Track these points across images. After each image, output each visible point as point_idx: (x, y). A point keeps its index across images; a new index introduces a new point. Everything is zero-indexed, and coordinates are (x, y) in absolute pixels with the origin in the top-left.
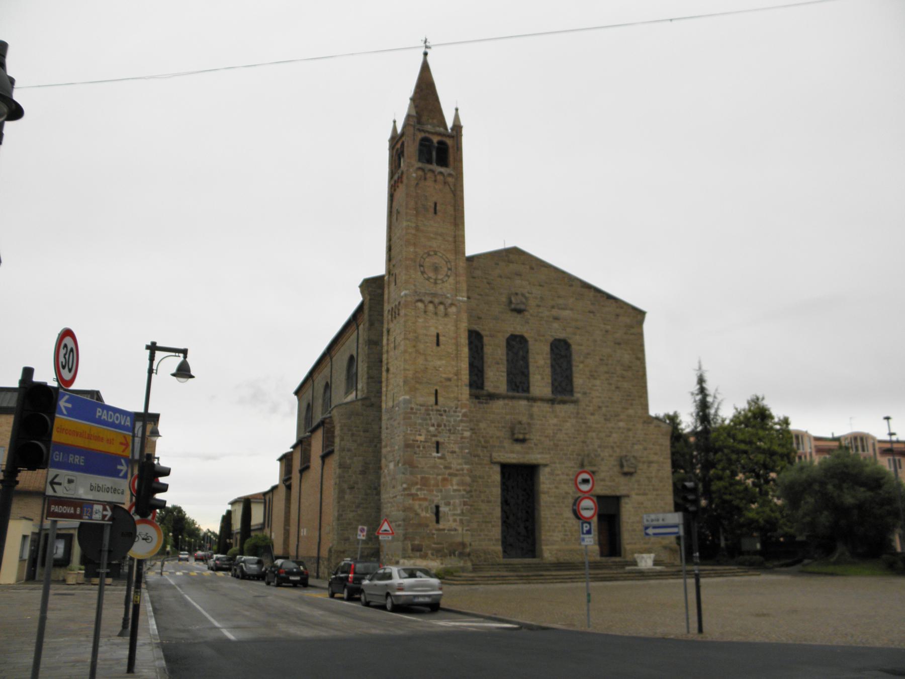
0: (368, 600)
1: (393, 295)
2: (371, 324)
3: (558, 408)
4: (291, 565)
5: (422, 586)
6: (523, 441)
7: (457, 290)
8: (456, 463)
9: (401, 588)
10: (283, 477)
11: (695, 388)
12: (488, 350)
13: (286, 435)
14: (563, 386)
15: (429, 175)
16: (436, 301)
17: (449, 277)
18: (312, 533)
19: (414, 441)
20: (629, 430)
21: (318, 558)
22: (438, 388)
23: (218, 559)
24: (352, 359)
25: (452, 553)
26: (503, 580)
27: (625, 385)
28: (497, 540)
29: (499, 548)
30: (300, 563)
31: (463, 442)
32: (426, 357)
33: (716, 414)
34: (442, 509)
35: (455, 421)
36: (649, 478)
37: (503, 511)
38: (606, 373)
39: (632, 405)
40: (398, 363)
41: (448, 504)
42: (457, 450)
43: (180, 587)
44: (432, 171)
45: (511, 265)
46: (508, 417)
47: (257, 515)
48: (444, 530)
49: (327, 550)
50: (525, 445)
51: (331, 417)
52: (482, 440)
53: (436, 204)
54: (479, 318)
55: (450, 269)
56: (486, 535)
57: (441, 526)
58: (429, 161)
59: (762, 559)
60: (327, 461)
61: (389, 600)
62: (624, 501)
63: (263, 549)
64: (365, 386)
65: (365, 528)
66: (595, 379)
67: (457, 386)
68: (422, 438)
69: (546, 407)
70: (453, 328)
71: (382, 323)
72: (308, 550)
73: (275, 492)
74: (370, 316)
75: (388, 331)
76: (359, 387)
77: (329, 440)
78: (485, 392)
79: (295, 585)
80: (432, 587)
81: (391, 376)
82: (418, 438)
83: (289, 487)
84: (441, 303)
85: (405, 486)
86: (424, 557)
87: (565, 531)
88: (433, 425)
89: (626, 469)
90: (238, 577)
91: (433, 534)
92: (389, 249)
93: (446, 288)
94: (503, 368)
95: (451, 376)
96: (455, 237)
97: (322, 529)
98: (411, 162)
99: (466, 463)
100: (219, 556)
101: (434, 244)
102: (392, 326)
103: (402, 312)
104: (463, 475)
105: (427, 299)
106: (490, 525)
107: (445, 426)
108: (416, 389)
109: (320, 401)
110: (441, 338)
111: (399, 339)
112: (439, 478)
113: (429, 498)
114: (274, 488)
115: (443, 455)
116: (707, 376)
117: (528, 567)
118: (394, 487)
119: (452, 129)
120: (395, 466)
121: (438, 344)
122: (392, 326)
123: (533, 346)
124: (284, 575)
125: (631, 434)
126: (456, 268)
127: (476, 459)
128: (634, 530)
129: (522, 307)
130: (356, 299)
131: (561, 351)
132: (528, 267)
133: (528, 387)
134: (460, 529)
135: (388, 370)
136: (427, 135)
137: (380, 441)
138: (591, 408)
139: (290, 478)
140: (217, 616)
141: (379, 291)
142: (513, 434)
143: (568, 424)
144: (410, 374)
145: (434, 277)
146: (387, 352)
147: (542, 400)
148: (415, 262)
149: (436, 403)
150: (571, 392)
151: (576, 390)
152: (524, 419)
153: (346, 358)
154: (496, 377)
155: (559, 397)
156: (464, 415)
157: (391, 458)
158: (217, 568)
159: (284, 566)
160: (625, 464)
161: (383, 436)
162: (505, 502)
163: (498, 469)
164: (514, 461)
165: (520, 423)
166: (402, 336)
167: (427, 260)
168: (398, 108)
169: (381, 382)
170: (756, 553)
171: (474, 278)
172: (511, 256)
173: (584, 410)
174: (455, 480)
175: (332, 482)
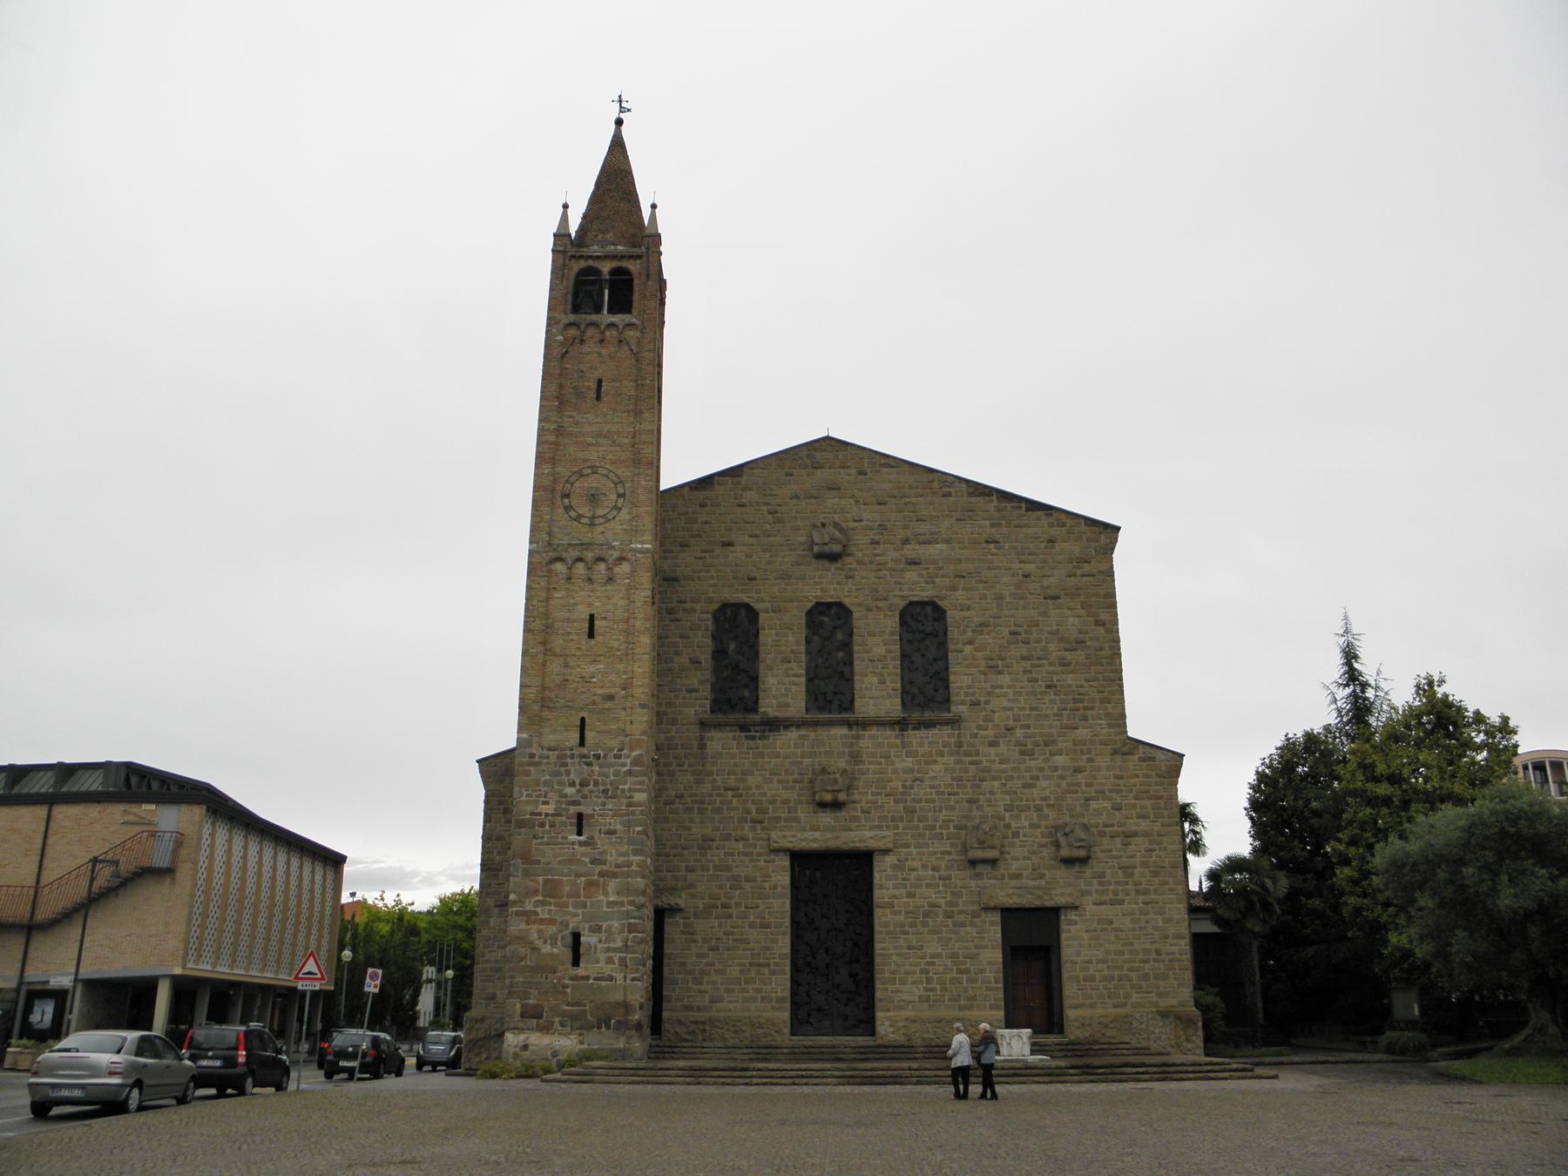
3: (914, 736)
6: (836, 805)
14: (927, 691)
16: (589, 555)
17: (620, 509)
20: (1077, 770)
22: (585, 715)
25: (603, 1022)
28: (780, 1000)
29: (786, 1015)
31: (633, 813)
35: (617, 774)
36: (1127, 870)
38: (1023, 658)
39: (1085, 718)
41: (596, 929)
42: (619, 827)
46: (807, 761)
48: (587, 978)
50: (843, 814)
53: (600, 382)
55: (620, 496)
56: (758, 990)
57: (580, 972)
59: (1418, 1036)
65: (380, 972)
66: (1000, 673)
67: (624, 709)
68: (550, 809)
69: (889, 736)
70: (622, 603)
78: (757, 718)
82: (543, 809)
86: (546, 1029)
87: (929, 981)
88: (572, 784)
89: (1065, 853)
94: (799, 668)
95: (613, 691)
99: (636, 852)
101: (593, 454)
106: (766, 970)
107: (596, 783)
108: (542, 719)
115: (591, 838)
121: (591, 635)
123: (861, 622)
124: (330, 1057)
125: (1080, 778)
127: (741, 844)
131: (924, 628)
132: (854, 471)
134: (619, 977)
136: (590, 262)
138: (990, 732)
145: (589, 514)
147: (880, 723)
148: (553, 491)
149: (582, 743)
151: (953, 698)
156: (636, 762)
162: (799, 928)
164: (815, 846)
170: (1411, 1024)
173: (975, 736)
174: (612, 885)
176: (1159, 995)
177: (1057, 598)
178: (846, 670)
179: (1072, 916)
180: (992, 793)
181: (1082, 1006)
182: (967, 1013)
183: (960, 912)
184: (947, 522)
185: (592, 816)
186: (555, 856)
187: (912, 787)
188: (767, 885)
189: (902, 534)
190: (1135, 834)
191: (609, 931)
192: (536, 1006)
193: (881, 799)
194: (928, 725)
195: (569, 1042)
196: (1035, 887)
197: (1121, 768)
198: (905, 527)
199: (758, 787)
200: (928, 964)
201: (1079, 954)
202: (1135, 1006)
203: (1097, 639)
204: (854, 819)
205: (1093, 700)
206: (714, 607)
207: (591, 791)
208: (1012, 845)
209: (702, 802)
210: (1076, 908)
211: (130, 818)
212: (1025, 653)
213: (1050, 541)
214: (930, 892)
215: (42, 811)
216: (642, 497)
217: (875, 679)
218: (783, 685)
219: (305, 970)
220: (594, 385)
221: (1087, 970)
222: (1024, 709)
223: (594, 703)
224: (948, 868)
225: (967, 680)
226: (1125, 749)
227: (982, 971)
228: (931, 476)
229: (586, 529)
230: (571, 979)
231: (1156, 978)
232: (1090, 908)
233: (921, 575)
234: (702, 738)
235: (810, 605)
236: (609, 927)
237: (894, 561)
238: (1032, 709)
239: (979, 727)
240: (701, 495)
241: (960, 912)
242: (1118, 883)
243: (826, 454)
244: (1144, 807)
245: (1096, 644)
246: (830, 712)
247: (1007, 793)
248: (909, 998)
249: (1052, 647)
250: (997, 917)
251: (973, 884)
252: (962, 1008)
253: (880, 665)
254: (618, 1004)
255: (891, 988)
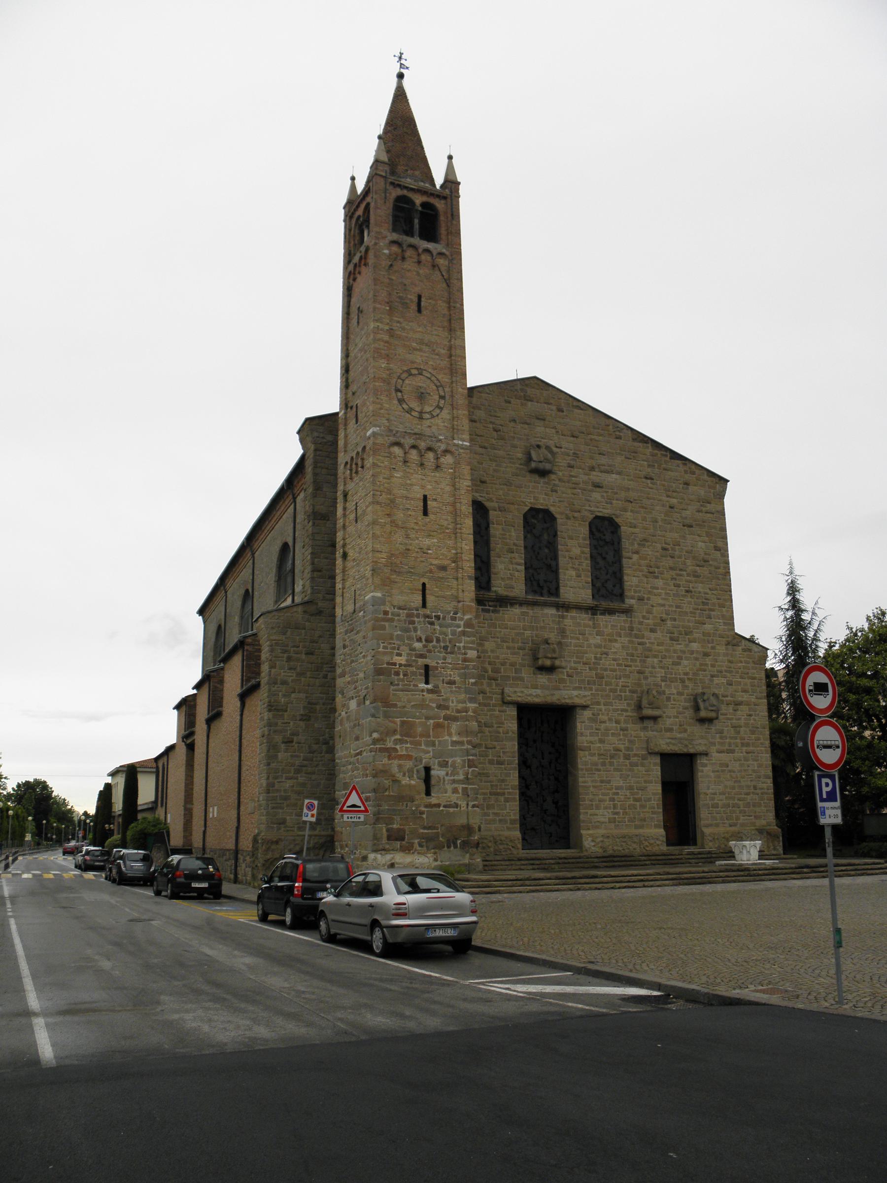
0: (333, 931)
1: (350, 439)
2: (318, 488)
3: (602, 619)
4: (191, 864)
5: (441, 907)
6: (551, 669)
7: (454, 430)
8: (455, 700)
9: (401, 912)
10: (183, 732)
11: (784, 600)
12: (496, 531)
13: (186, 673)
14: (609, 589)
15: (409, 253)
16: (422, 445)
17: (441, 409)
18: (229, 814)
19: (388, 663)
20: (706, 655)
21: (237, 852)
22: (426, 581)
23: (88, 853)
24: (285, 549)
25: (451, 843)
26: (536, 885)
27: (700, 587)
28: (513, 822)
29: (517, 834)
30: (208, 861)
31: (467, 667)
32: (407, 539)
33: (815, 639)
34: (435, 772)
35: (454, 633)
37: (521, 777)
38: (671, 568)
39: (709, 617)
40: (362, 543)
42: (457, 679)
43: (12, 903)
44: (413, 247)
45: (530, 403)
46: (528, 633)
47: (146, 791)
48: (439, 805)
49: (251, 838)
50: (554, 676)
51: (255, 635)
52: (489, 668)
53: (420, 297)
54: (483, 482)
56: (495, 814)
58: (409, 233)
60: (249, 702)
61: (378, 934)
62: (701, 761)
63: (152, 838)
64: (308, 583)
66: (657, 577)
68: (402, 660)
69: (584, 618)
70: (448, 489)
71: (335, 486)
72: (220, 839)
73: (171, 754)
74: (315, 475)
75: (345, 495)
76: (298, 588)
77: (251, 670)
79: (200, 896)
80: (459, 909)
81: (349, 564)
82: (397, 659)
83: (191, 747)
84: (430, 449)
85: (375, 735)
86: (408, 849)
87: (615, 807)
88: (419, 640)
89: (703, 714)
90: (114, 881)
91: (422, 813)
92: (346, 369)
93: (437, 426)
95: (446, 562)
96: (450, 348)
97: (242, 808)
98: (381, 235)
99: (471, 700)
100: (92, 848)
101: (418, 358)
102: (351, 486)
103: (369, 462)
104: (466, 719)
105: (408, 441)
106: (502, 798)
107: (438, 641)
109: (237, 619)
110: (430, 503)
111: (362, 506)
112: (424, 724)
113: (414, 754)
114: (170, 749)
115: (436, 686)
116: (801, 583)
117: (564, 863)
118: (357, 739)
119: (442, 186)
120: (359, 705)
121: (425, 513)
122: (351, 486)
123: (564, 527)
124: (182, 880)
125: (708, 661)
126: (452, 396)
128: (716, 806)
129: (548, 466)
130: (292, 452)
132: (554, 408)
133: (557, 588)
134: (463, 804)
135: (345, 556)
136: (405, 192)
137: (333, 668)
139: (192, 734)
140: (46, 974)
141: (330, 438)
142: (536, 659)
143: (618, 645)
144: (383, 558)
146: (344, 527)
147: (579, 607)
149: (424, 605)
150: (621, 596)
151: (627, 593)
152: (553, 637)
153: (276, 548)
154: (509, 574)
155: (604, 604)
156: (468, 624)
157: (351, 693)
158: (85, 867)
159: (182, 866)
160: (702, 705)
161: (338, 660)
162: (524, 764)
163: (513, 712)
164: (537, 700)
165: (546, 642)
166: (369, 499)
167: (407, 382)
168: (356, 156)
169: (333, 577)
171: (475, 421)
172: (530, 391)
173: (641, 623)
174: (455, 727)
175: (258, 733)
177: (691, 526)
178: (553, 563)
179: (704, 760)
180: (653, 667)
182: (641, 831)
184: (619, 459)
185: (436, 668)
186: (409, 701)
187: (601, 659)
188: (501, 730)
191: (454, 765)
192: (399, 830)
193: (580, 667)
194: (611, 612)
195: (426, 860)
196: (681, 739)
198: (591, 458)
199: (492, 651)
202: (742, 825)
204: (562, 681)
205: (714, 604)
207: (434, 647)
210: (706, 754)
214: (614, 739)
216: (460, 402)
217: (574, 573)
219: (349, 803)
220: (416, 299)
221: (713, 799)
223: (431, 571)
224: (626, 722)
225: (635, 580)
226: (735, 642)
227: (649, 800)
229: (416, 421)
230: (426, 806)
232: (715, 754)
233: (602, 496)
235: (527, 508)
236: (454, 762)
238: (677, 607)
239: (644, 617)
241: (635, 755)
242: (731, 738)
244: (746, 684)
245: (715, 564)
246: (542, 595)
248: (602, 820)
249: (689, 562)
250: (657, 760)
252: (637, 827)
253: (577, 562)
254: (463, 826)
255: (590, 812)
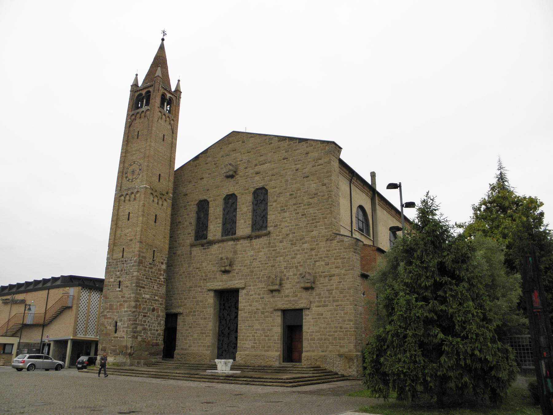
3: (255, 241)
14: (260, 223)
16: (129, 192)
20: (312, 249)
22: (124, 247)
27: (311, 211)
28: (208, 346)
31: (133, 280)
38: (294, 204)
41: (121, 320)
42: (129, 285)
48: (117, 337)
50: (230, 275)
52: (204, 275)
56: (202, 343)
57: (116, 335)
62: (305, 313)
69: (246, 243)
88: (119, 271)
94: (220, 221)
99: (133, 293)
106: (204, 335)
115: (122, 289)
125: (313, 253)
128: (313, 339)
134: (125, 337)
138: (280, 237)
149: (123, 257)
173: (275, 239)
174: (126, 305)
176: (341, 347)
177: (308, 177)
180: (280, 262)
181: (309, 351)
183: (267, 312)
184: (270, 155)
187: (253, 262)
189: (255, 162)
190: (334, 275)
193: (242, 268)
197: (329, 247)
198: (256, 160)
199: (206, 267)
200: (255, 333)
201: (309, 329)
202: (330, 351)
203: (323, 192)
204: (234, 276)
205: (319, 218)
206: (197, 202)
208: (286, 283)
209: (190, 274)
210: (309, 309)
211: (64, 292)
212: (295, 202)
213: (307, 154)
215: (47, 291)
217: (243, 221)
218: (215, 229)
220: (136, 134)
221: (312, 335)
222: (293, 226)
224: (263, 294)
228: (265, 138)
231: (340, 339)
233: (260, 178)
234: (191, 251)
235: (224, 196)
237: (251, 174)
240: (195, 163)
242: (326, 297)
243: (234, 138)
244: (338, 263)
245: (322, 194)
247: (285, 262)
248: (248, 346)
249: (305, 198)
250: (279, 313)
251: (272, 300)
252: (266, 351)
